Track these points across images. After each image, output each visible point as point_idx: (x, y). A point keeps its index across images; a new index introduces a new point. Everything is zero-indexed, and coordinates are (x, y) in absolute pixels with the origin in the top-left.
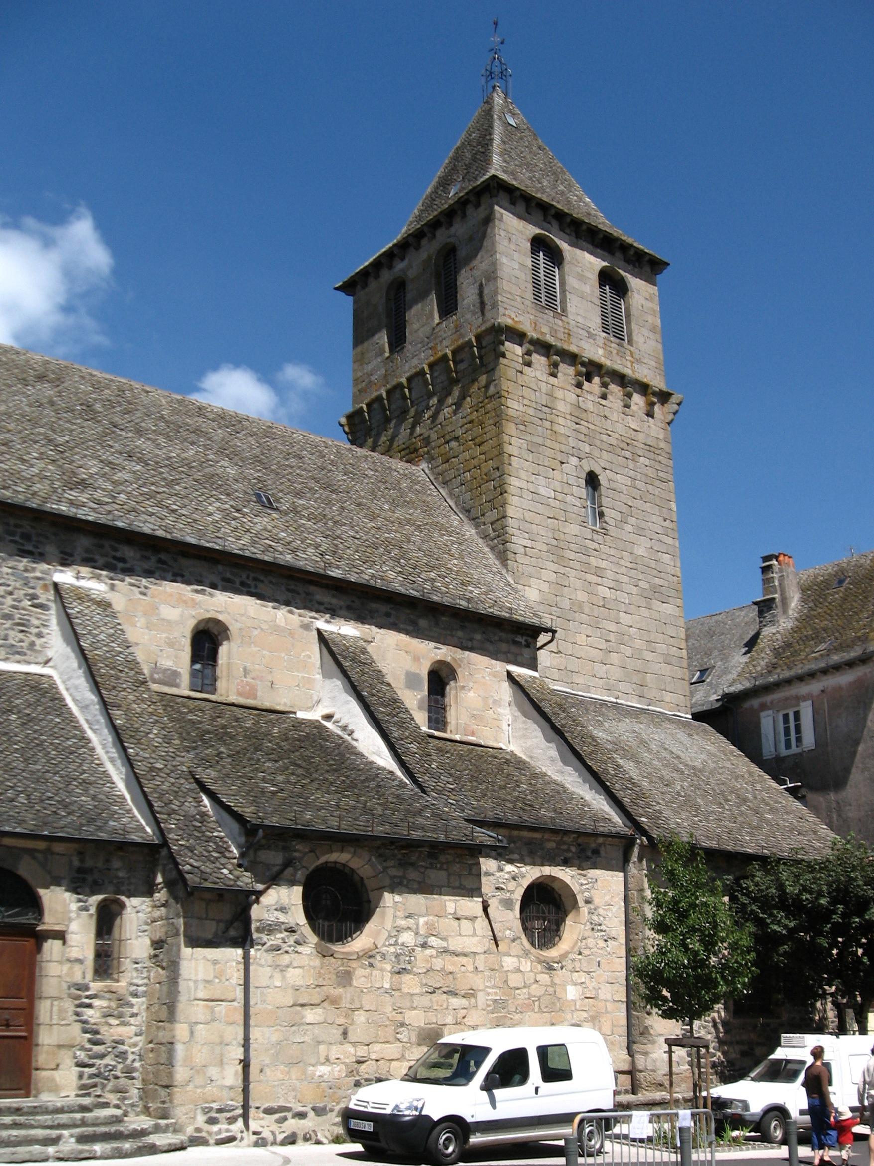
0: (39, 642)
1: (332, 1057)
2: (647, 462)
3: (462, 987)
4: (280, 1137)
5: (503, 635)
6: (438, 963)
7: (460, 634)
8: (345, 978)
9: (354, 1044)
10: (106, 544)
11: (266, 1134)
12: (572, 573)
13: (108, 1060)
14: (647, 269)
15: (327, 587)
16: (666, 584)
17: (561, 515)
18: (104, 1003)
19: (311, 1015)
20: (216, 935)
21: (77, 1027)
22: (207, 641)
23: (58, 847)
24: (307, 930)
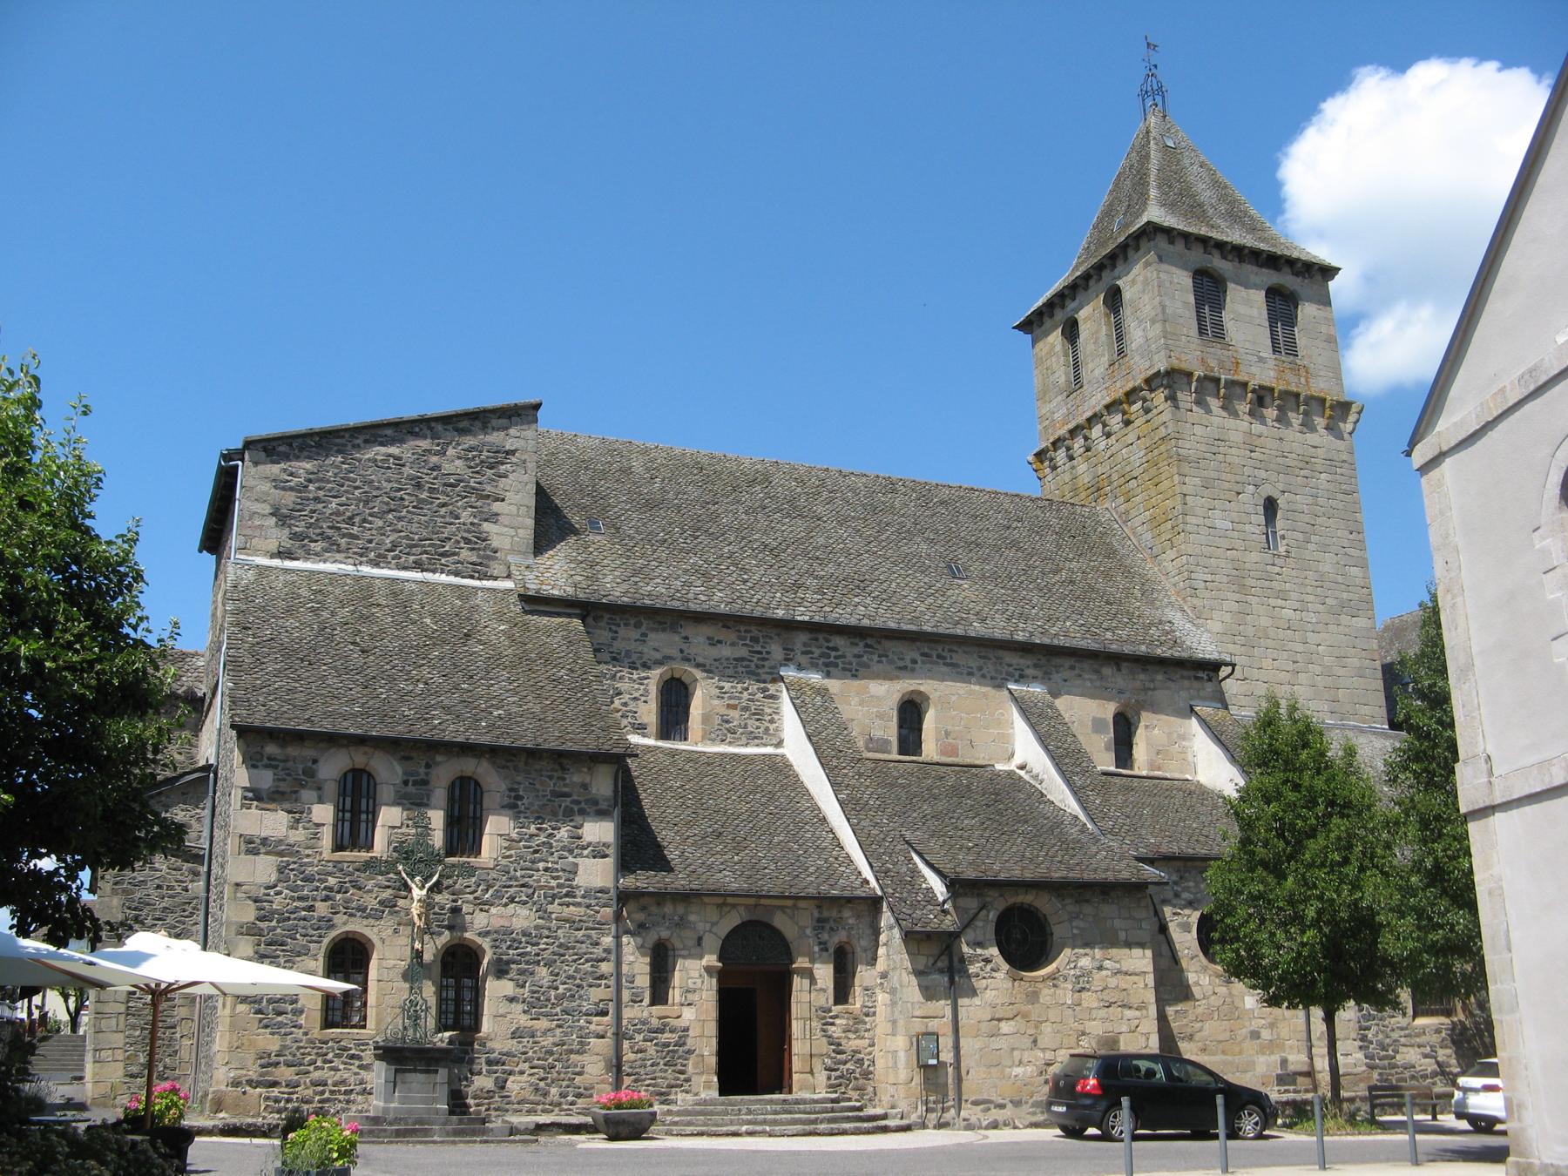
0: (772, 727)
1: (1025, 1060)
2: (1330, 477)
3: (1135, 1001)
4: (985, 1123)
5: (1185, 673)
6: (1113, 982)
7: (1142, 677)
8: (1033, 997)
9: (1043, 1050)
10: (821, 637)
11: (973, 1119)
12: (1253, 600)
13: (848, 1066)
14: (1319, 277)
15: (1015, 650)
16: (1356, 597)
17: (1238, 544)
18: (844, 1022)
19: (1005, 1027)
20: (926, 966)
21: (825, 1040)
22: (911, 713)
23: (802, 904)
24: (1000, 960)
